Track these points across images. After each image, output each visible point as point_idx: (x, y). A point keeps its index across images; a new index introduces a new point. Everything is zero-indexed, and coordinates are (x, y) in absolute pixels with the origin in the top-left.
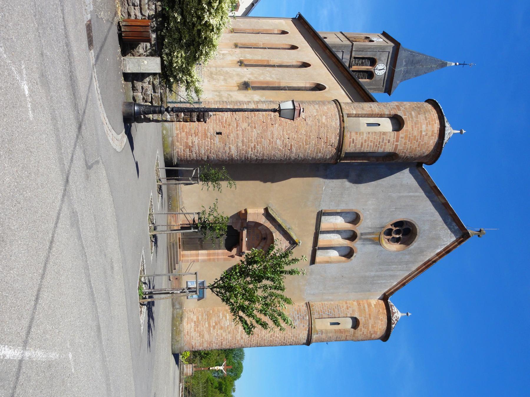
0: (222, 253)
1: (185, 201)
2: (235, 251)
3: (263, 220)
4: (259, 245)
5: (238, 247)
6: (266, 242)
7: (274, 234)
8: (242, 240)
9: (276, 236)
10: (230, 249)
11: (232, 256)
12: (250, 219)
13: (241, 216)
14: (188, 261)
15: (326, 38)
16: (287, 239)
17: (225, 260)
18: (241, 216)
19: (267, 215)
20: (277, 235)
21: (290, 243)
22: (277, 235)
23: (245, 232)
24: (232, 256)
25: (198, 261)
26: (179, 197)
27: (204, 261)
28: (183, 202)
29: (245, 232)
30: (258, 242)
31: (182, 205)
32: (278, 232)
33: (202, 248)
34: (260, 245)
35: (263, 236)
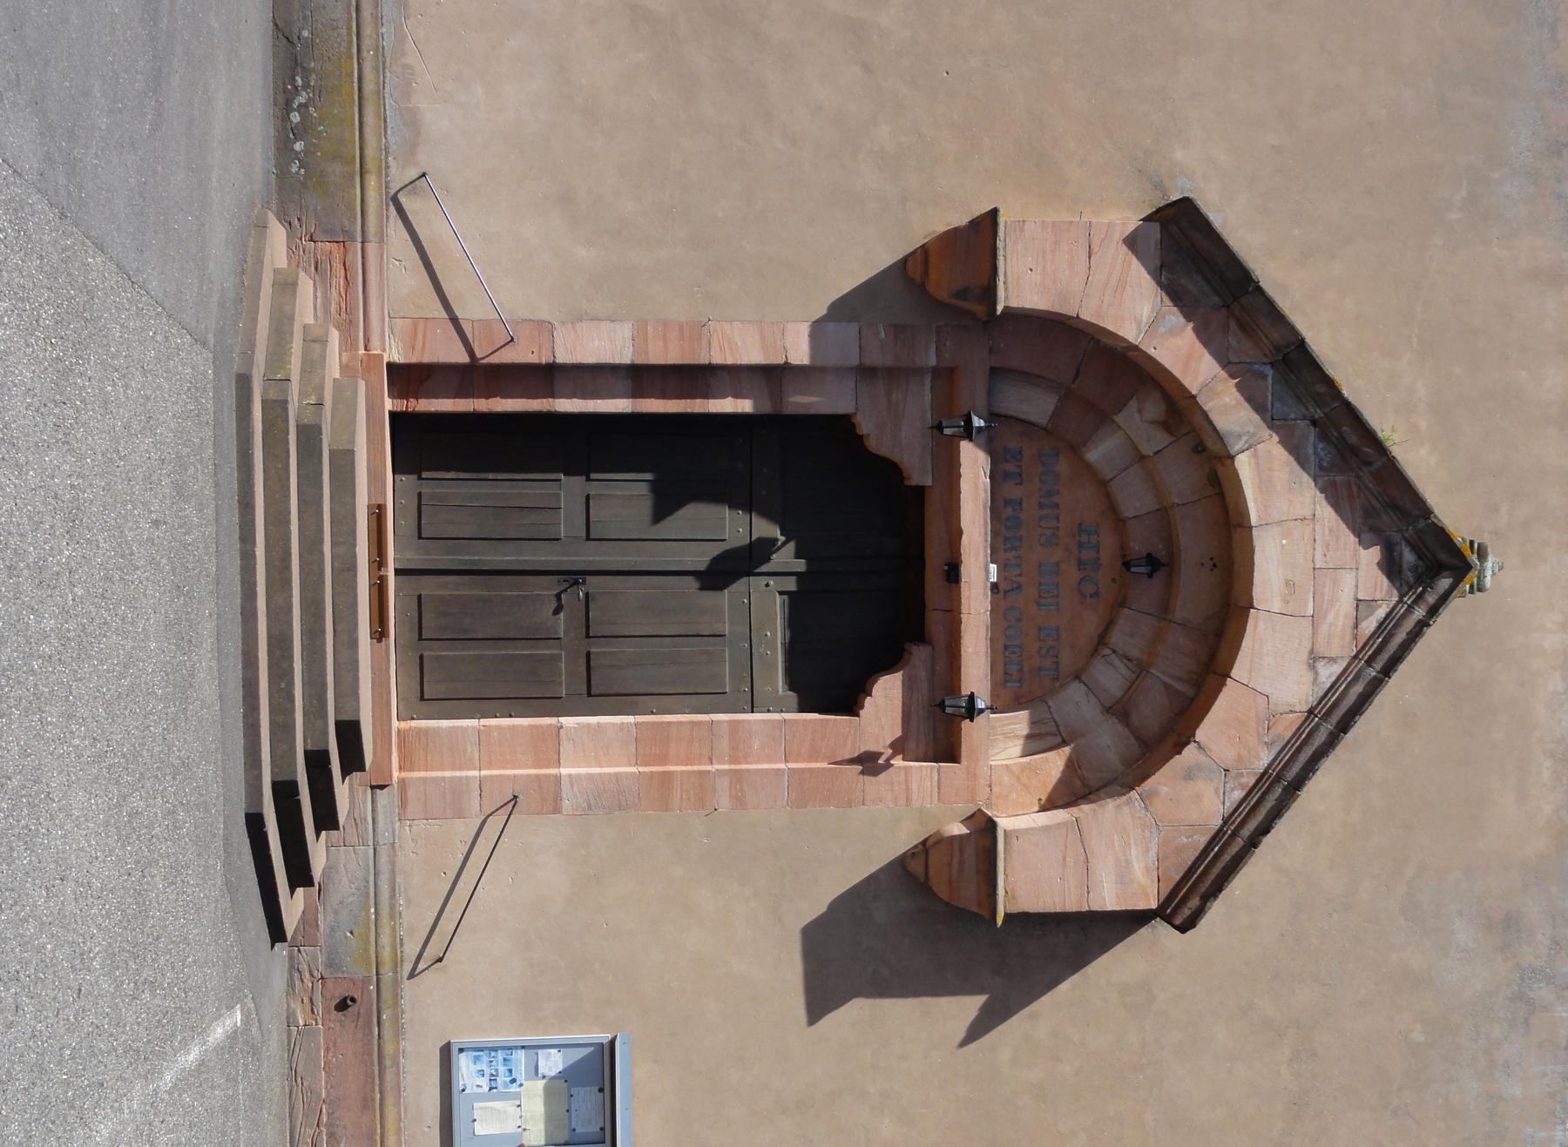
0: (774, 739)
1: (436, 118)
2: (887, 697)
3: (1135, 308)
4: (1102, 640)
5: (919, 655)
6: (1164, 610)
7: (1244, 465)
8: (953, 573)
9: (1264, 485)
10: (841, 696)
11: (869, 763)
12: (1024, 283)
13: (945, 286)
14: (453, 800)
15: (976, 1031)
16: (1366, 525)
17: (803, 790)
18: (945, 286)
19: (1185, 248)
20: (1275, 486)
21: (1391, 567)
22: (1275, 486)
23: (974, 464)
24: (869, 763)
25: (550, 797)
26: (381, 67)
27: (609, 800)
28: (413, 122)
29: (974, 464)
30: (1091, 623)
31: (411, 150)
32: (1273, 448)
33: (596, 695)
34: (1117, 637)
35: (1137, 547)
